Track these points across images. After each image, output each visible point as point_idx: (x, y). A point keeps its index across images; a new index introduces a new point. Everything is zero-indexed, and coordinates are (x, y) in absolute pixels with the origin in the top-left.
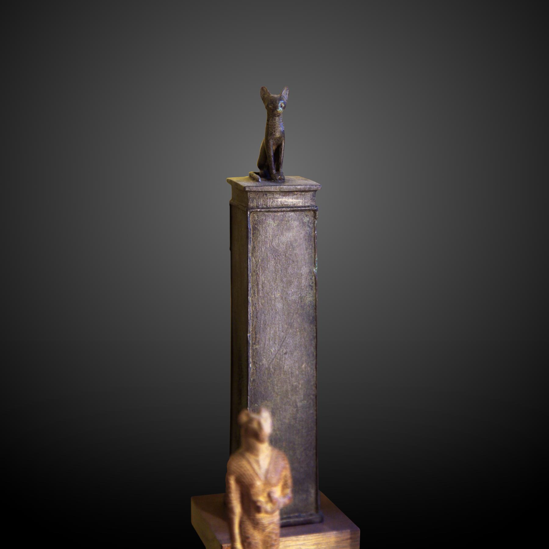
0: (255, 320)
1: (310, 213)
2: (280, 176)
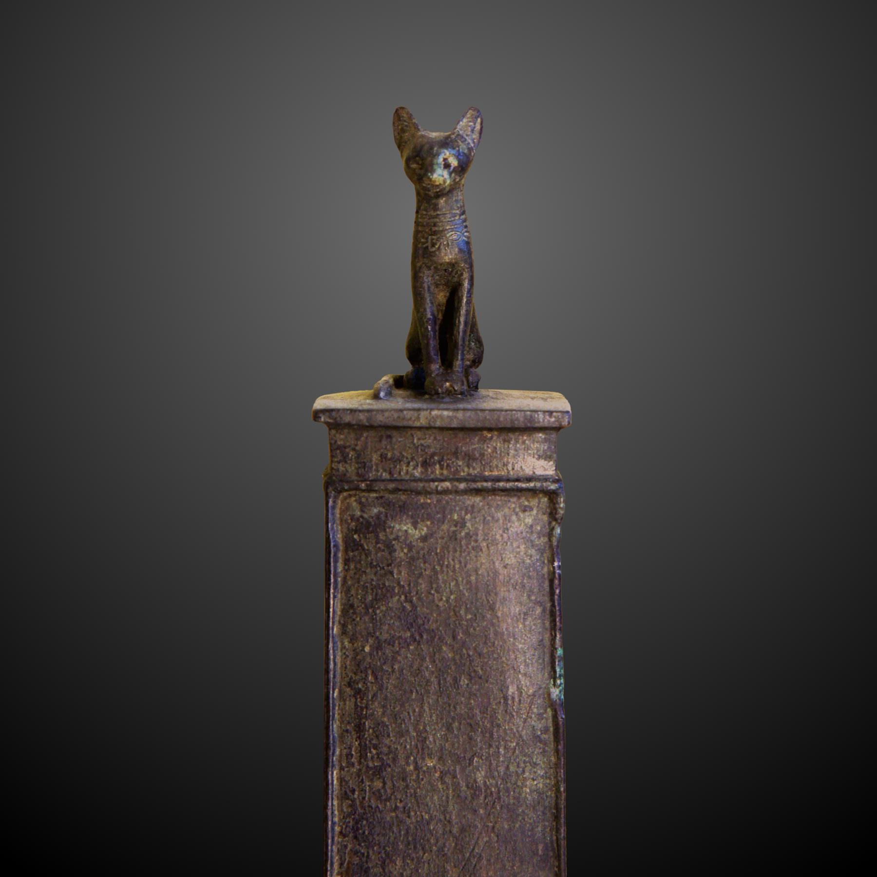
0: (350, 846)
1: (537, 500)
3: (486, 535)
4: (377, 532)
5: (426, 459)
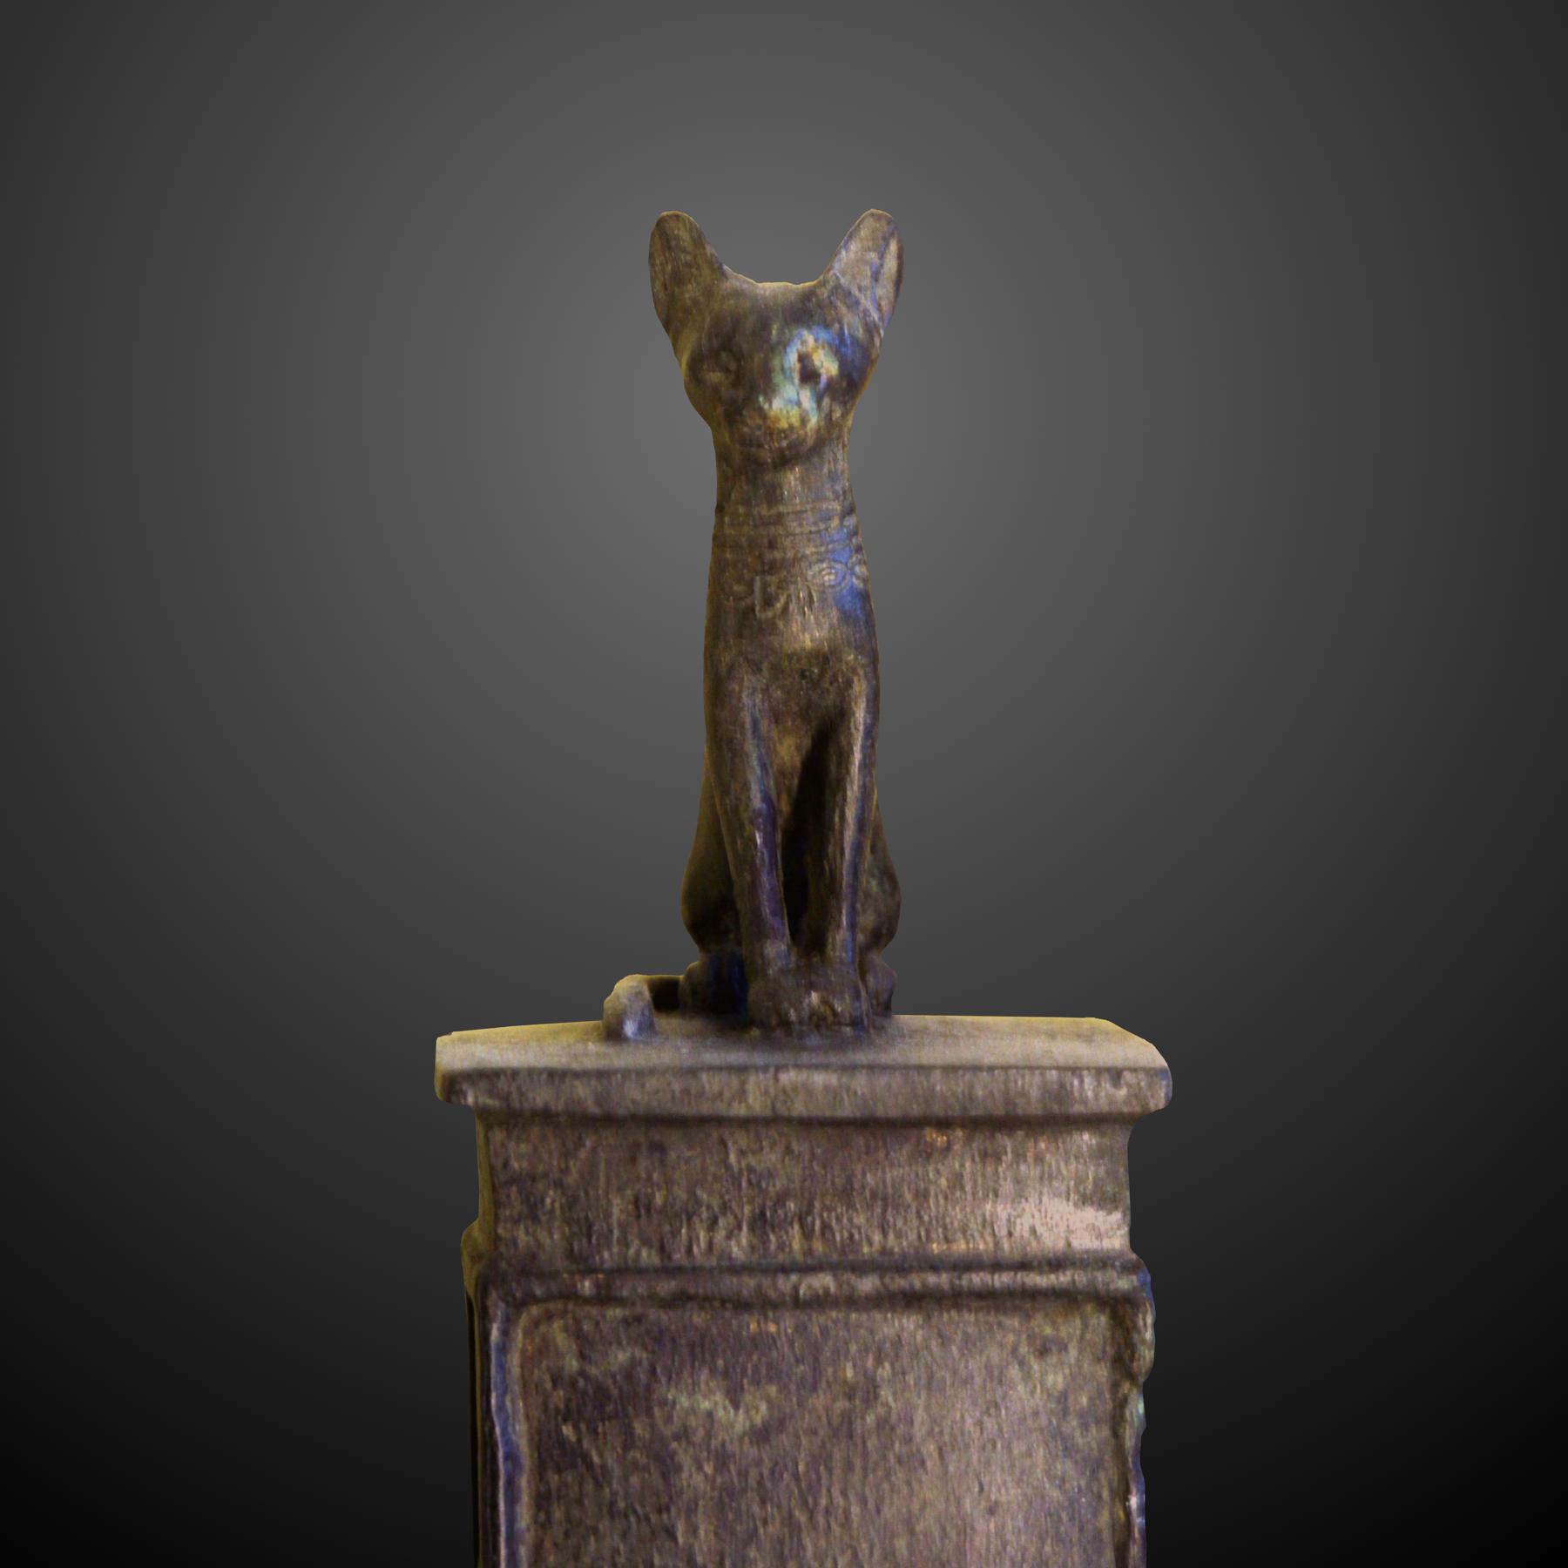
1: (1078, 1322)
2: (815, 997)
3: (934, 1421)
4: (627, 1416)
5: (763, 1207)
